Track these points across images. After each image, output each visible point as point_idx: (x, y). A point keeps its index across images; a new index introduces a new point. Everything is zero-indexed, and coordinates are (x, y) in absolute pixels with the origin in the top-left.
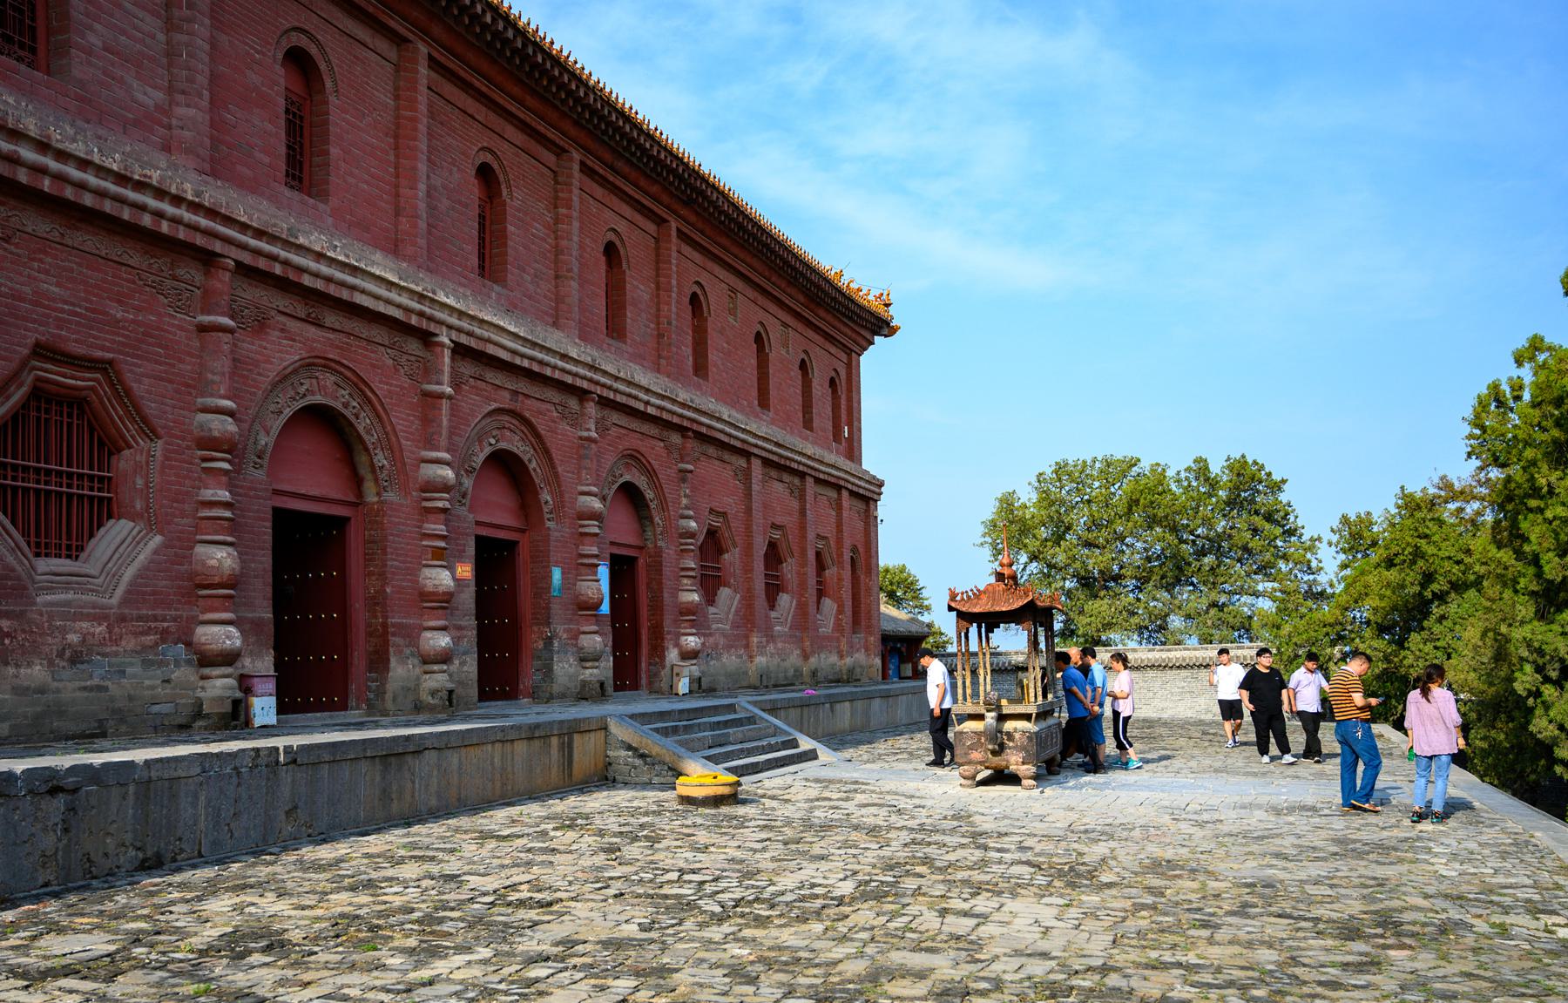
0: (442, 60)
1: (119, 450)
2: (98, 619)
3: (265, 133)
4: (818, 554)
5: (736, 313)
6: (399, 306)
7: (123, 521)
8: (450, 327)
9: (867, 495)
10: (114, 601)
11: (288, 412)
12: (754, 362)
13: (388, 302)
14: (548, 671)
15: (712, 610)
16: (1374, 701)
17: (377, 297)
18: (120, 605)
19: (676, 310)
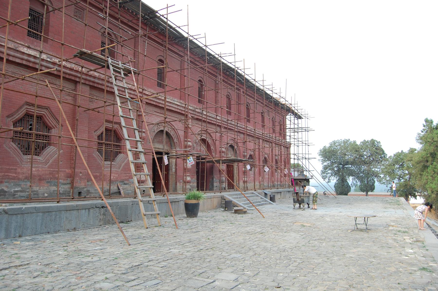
0: (170, 48)
1: (52, 129)
2: (117, 174)
3: (244, 115)
4: (276, 160)
5: (257, 108)
6: (180, 110)
7: (51, 147)
8: (191, 113)
9: (288, 147)
10: (120, 170)
11: (156, 132)
12: (261, 118)
13: (178, 109)
14: (213, 185)
15: (251, 172)
16: (200, 282)
17: (175, 108)
18: (121, 171)
19: (243, 109)
